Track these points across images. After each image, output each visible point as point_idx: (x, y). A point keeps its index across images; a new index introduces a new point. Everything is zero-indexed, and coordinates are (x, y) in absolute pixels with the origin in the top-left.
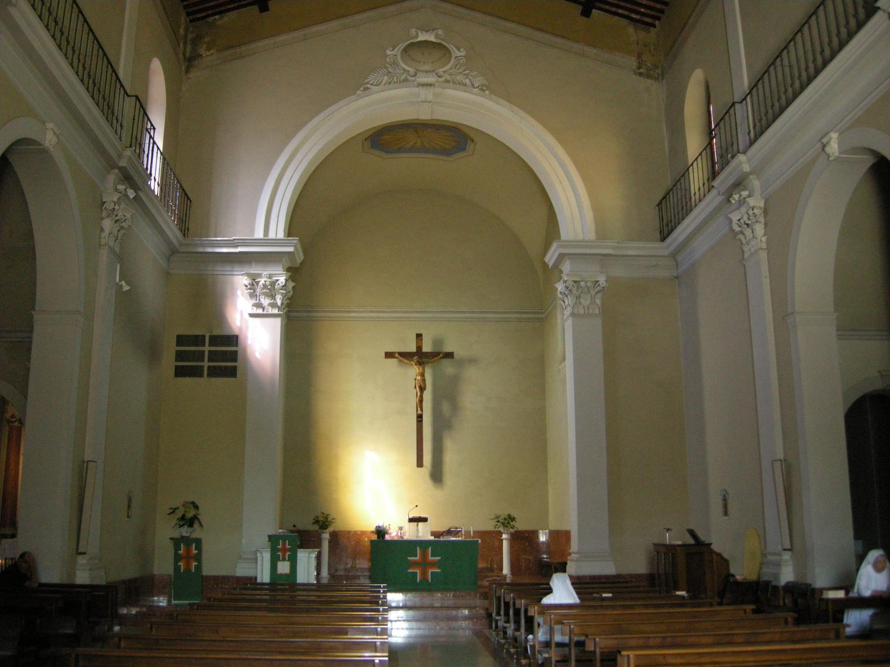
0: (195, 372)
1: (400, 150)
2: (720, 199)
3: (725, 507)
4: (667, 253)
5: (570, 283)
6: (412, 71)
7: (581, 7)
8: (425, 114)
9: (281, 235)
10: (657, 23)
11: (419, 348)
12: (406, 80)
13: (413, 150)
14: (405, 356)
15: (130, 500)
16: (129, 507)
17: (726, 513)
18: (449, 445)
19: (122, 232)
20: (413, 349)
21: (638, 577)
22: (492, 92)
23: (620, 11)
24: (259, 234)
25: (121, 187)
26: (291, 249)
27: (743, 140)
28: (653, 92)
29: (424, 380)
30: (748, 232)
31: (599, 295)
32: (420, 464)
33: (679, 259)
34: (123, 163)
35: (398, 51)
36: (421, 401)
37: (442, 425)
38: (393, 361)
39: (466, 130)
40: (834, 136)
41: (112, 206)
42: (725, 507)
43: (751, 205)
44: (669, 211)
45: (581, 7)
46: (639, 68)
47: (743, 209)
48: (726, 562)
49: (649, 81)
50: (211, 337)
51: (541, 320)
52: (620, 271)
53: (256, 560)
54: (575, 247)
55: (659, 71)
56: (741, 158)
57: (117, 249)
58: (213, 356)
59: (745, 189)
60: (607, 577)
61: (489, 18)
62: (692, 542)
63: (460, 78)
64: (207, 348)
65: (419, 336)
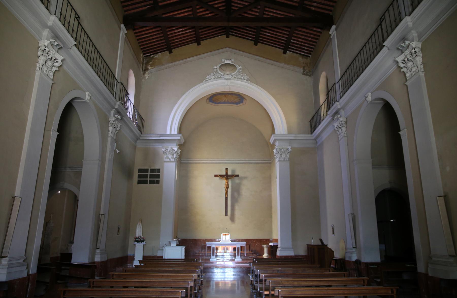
0: (145, 182)
1: (220, 103)
2: (331, 118)
3: (333, 231)
4: (313, 138)
5: (278, 150)
6: (223, 74)
7: (253, 42)
8: (227, 90)
9: (176, 133)
10: (310, 55)
11: (227, 173)
12: (220, 77)
13: (225, 102)
14: (221, 176)
15: (119, 228)
16: (118, 231)
17: (333, 233)
18: (237, 207)
19: (117, 132)
20: (225, 174)
21: (302, 256)
22: (251, 82)
23: (297, 52)
24: (168, 133)
25: (116, 116)
26: (179, 138)
27: (338, 97)
28: (309, 80)
29: (228, 185)
30: (340, 130)
31: (289, 154)
32: (226, 215)
33: (317, 141)
34: (117, 107)
35: (218, 67)
36: (227, 193)
37: (235, 200)
38: (217, 178)
39: (243, 96)
40: (370, 94)
41: (112, 122)
42: (333, 231)
43: (341, 120)
44: (314, 122)
45: (253, 42)
46: (304, 72)
47: (338, 122)
48: (333, 252)
49: (307, 77)
50: (150, 169)
51: (270, 163)
52: (296, 145)
53: (163, 250)
54: (283, 136)
55: (311, 73)
56: (337, 103)
57: (115, 138)
58: (151, 176)
59: (339, 114)
60: (291, 256)
61: (251, 55)
62: (320, 244)
63: (240, 76)
64: (149, 174)
65: (227, 169)
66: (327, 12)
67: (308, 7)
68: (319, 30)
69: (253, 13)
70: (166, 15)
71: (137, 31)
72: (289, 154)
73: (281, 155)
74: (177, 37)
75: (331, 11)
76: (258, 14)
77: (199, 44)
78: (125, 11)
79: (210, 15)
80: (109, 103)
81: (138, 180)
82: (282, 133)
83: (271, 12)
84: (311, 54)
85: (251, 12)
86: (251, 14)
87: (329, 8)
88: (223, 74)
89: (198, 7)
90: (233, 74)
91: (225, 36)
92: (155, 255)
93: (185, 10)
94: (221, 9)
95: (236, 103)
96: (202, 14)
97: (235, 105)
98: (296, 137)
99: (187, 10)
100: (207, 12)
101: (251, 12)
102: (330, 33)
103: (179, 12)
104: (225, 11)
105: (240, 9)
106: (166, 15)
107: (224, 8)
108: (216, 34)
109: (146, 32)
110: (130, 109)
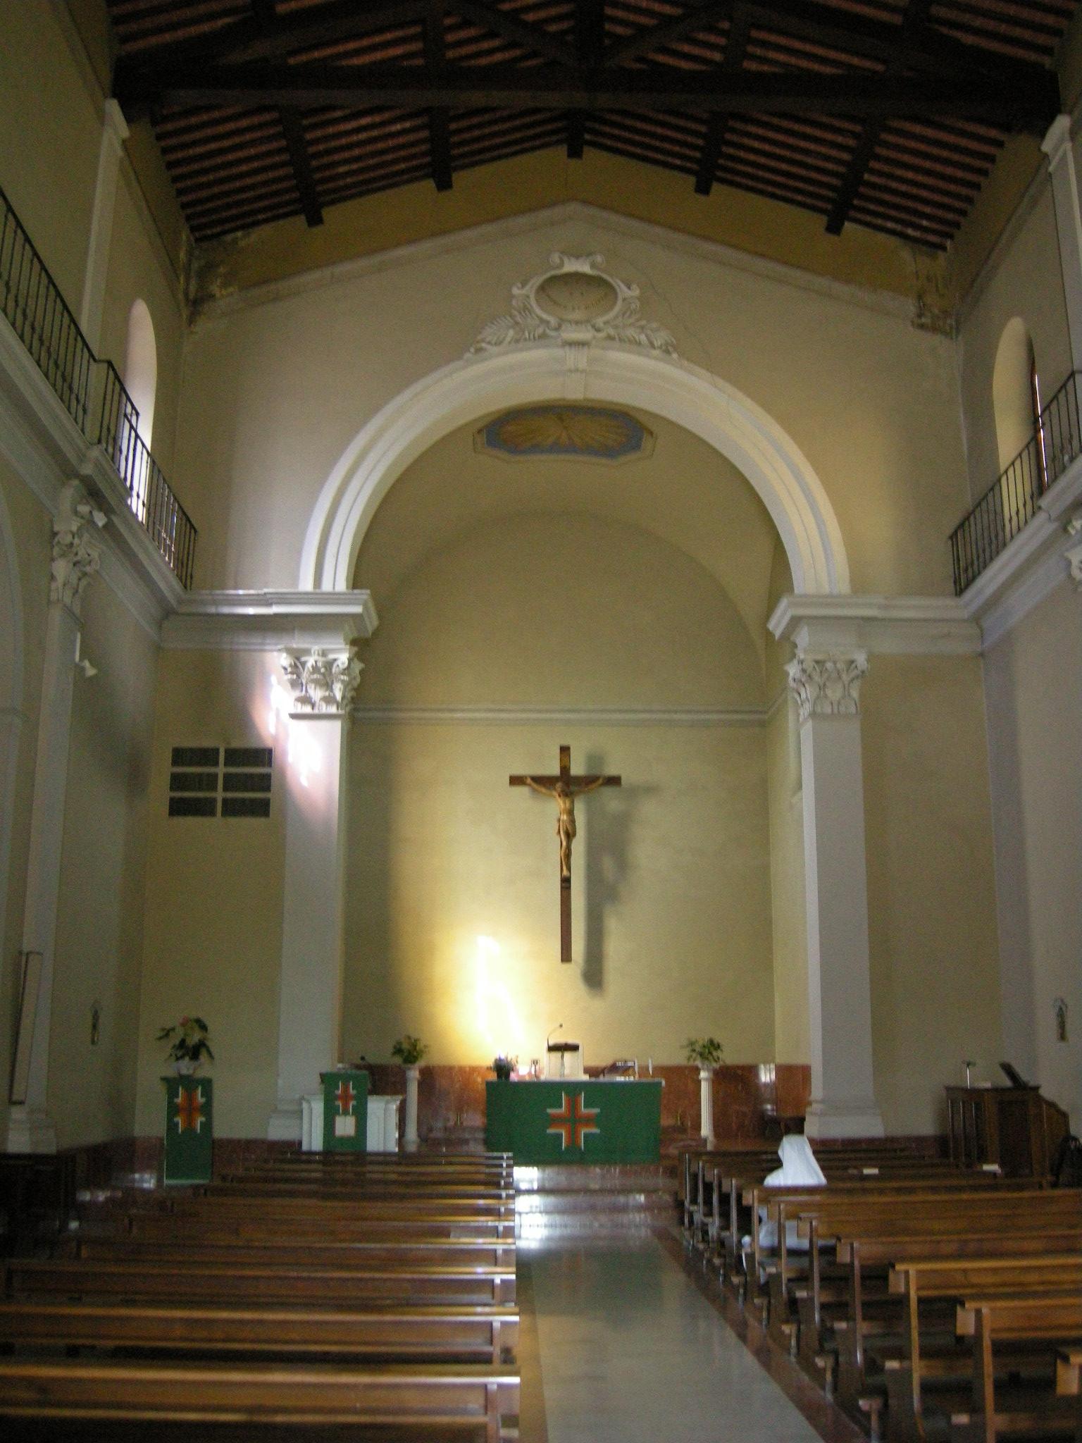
0: (202, 808)
1: (536, 449)
2: (1053, 526)
4: (965, 614)
5: (809, 665)
6: (553, 321)
8: (574, 391)
9: (342, 586)
10: (948, 243)
11: (565, 769)
13: (556, 448)
14: (542, 781)
15: (96, 1016)
16: (94, 1027)
17: (1062, 1037)
20: (555, 770)
21: (920, 1140)
22: (682, 355)
24: (306, 585)
25: (84, 509)
26: (358, 609)
28: (943, 353)
29: (573, 821)
31: (857, 684)
32: (566, 956)
35: (530, 289)
36: (568, 855)
38: (523, 791)
39: (643, 419)
41: (69, 539)
46: (920, 316)
48: (1064, 1116)
51: (763, 724)
52: (888, 645)
54: (828, 605)
60: (871, 1141)
63: (631, 332)
64: (221, 770)
65: (565, 750)
66: (1032, 56)
67: (945, 30)
68: (994, 133)
69: (696, 51)
70: (304, 58)
71: (169, 127)
72: (857, 684)
73: (822, 687)
74: (346, 155)
75: (1047, 50)
76: (717, 57)
77: (444, 184)
78: (125, 39)
79: (498, 57)
80: (53, 450)
81: (172, 799)
82: (826, 589)
83: (779, 51)
84: (951, 237)
85: (686, 48)
86: (694, 58)
87: (1042, 39)
88: (553, 321)
89: (448, 21)
90: (600, 321)
91: (562, 150)
92: (261, 1136)
93: (388, 36)
94: (553, 28)
95: (608, 452)
96: (464, 51)
97: (603, 461)
98: (886, 607)
99: (400, 33)
100: (486, 45)
101: (686, 48)
102: (1047, 146)
103: (365, 42)
104: (569, 38)
105: (642, 30)
106: (304, 58)
107: (565, 25)
108: (522, 140)
109: (209, 132)
110: (139, 475)
